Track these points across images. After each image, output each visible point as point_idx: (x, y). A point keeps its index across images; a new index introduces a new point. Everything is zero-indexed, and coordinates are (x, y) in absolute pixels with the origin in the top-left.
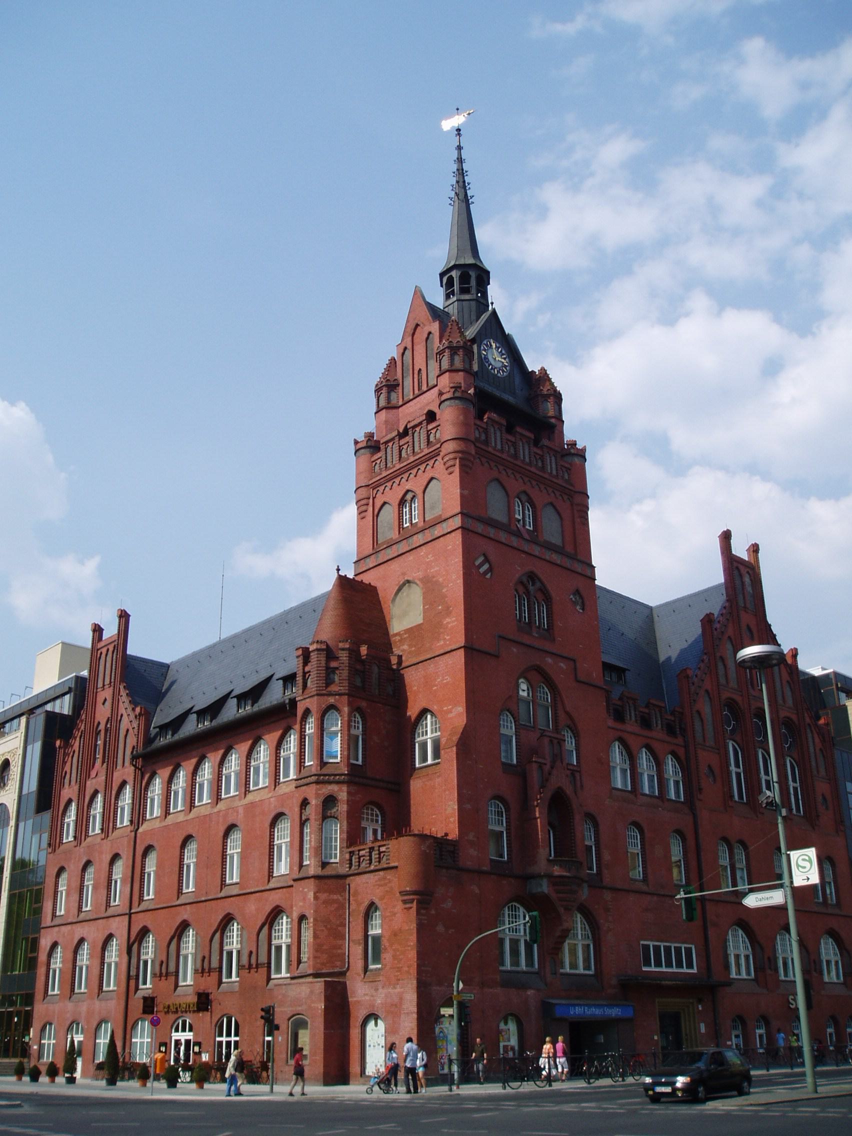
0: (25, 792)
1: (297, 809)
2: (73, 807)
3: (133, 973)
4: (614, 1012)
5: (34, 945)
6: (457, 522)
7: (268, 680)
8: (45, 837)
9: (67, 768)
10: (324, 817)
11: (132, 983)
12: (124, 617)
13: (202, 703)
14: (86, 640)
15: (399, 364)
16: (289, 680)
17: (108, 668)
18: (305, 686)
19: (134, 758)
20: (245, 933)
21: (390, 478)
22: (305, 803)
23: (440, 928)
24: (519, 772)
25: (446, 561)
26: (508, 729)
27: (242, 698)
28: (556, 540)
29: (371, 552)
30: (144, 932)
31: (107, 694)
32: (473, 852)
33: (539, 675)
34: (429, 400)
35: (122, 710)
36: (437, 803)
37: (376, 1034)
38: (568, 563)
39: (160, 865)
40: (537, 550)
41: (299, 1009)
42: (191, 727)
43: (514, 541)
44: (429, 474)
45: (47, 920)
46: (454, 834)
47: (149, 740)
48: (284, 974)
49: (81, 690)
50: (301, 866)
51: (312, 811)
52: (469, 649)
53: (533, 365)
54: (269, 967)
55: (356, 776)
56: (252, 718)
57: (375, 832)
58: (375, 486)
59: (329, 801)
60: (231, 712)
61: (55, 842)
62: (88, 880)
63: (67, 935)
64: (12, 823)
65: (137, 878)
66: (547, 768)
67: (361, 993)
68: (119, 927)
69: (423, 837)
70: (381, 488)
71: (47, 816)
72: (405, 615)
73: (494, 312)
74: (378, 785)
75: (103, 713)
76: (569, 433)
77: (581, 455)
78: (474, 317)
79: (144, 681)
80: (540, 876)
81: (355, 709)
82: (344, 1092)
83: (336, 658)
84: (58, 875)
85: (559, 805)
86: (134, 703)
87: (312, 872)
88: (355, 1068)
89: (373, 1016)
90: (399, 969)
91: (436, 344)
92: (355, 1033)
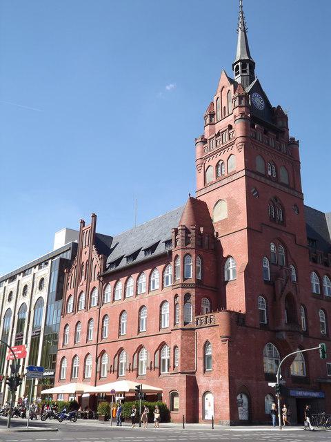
0: (51, 292)
1: (173, 299)
2: (72, 298)
3: (98, 370)
4: (315, 395)
5: (55, 357)
6: (243, 173)
7: (122, 257)
8: (60, 311)
9: (69, 281)
10: (185, 302)
11: (98, 374)
12: (94, 216)
13: (128, 253)
14: (77, 227)
15: (215, 104)
16: (168, 242)
17: (87, 239)
18: (176, 245)
19: (99, 277)
20: (149, 353)
21: (212, 155)
22: (176, 296)
23: (238, 353)
24: (272, 284)
25: (238, 191)
26: (266, 266)
27: (147, 251)
28: (286, 182)
29: (203, 187)
30: (103, 352)
31: (87, 249)
32: (252, 319)
33: (280, 242)
34: (229, 120)
35: (93, 257)
36: (236, 298)
37: (210, 398)
38: (292, 192)
39: (110, 323)
40: (278, 186)
41: (174, 388)
42: (124, 263)
43: (268, 182)
44: (230, 152)
45: (60, 347)
46: (243, 311)
47: (105, 269)
48: (166, 372)
49: (75, 249)
50: (175, 324)
51: (179, 300)
52: (249, 229)
53: (274, 105)
54: (160, 369)
55: (199, 284)
56: (153, 259)
57: (207, 309)
58: (205, 159)
59: (187, 296)
60: (141, 257)
61: (64, 313)
62: (143, 316)
63: (69, 354)
64: (45, 305)
65: (101, 329)
66: (284, 283)
67: (202, 381)
68: (92, 350)
69: (230, 312)
70: (208, 160)
71: (60, 302)
72: (219, 215)
73: (258, 81)
74: (209, 290)
75: (85, 258)
76: (292, 134)
77: (297, 144)
78: (248, 82)
79: (103, 245)
80: (282, 331)
81: (197, 254)
82: (194, 427)
83: (190, 233)
84: (65, 328)
85: (290, 299)
86: (99, 253)
87: (180, 327)
88: (200, 416)
89: (207, 392)
90: (220, 371)
91: (232, 95)
92: (200, 399)
